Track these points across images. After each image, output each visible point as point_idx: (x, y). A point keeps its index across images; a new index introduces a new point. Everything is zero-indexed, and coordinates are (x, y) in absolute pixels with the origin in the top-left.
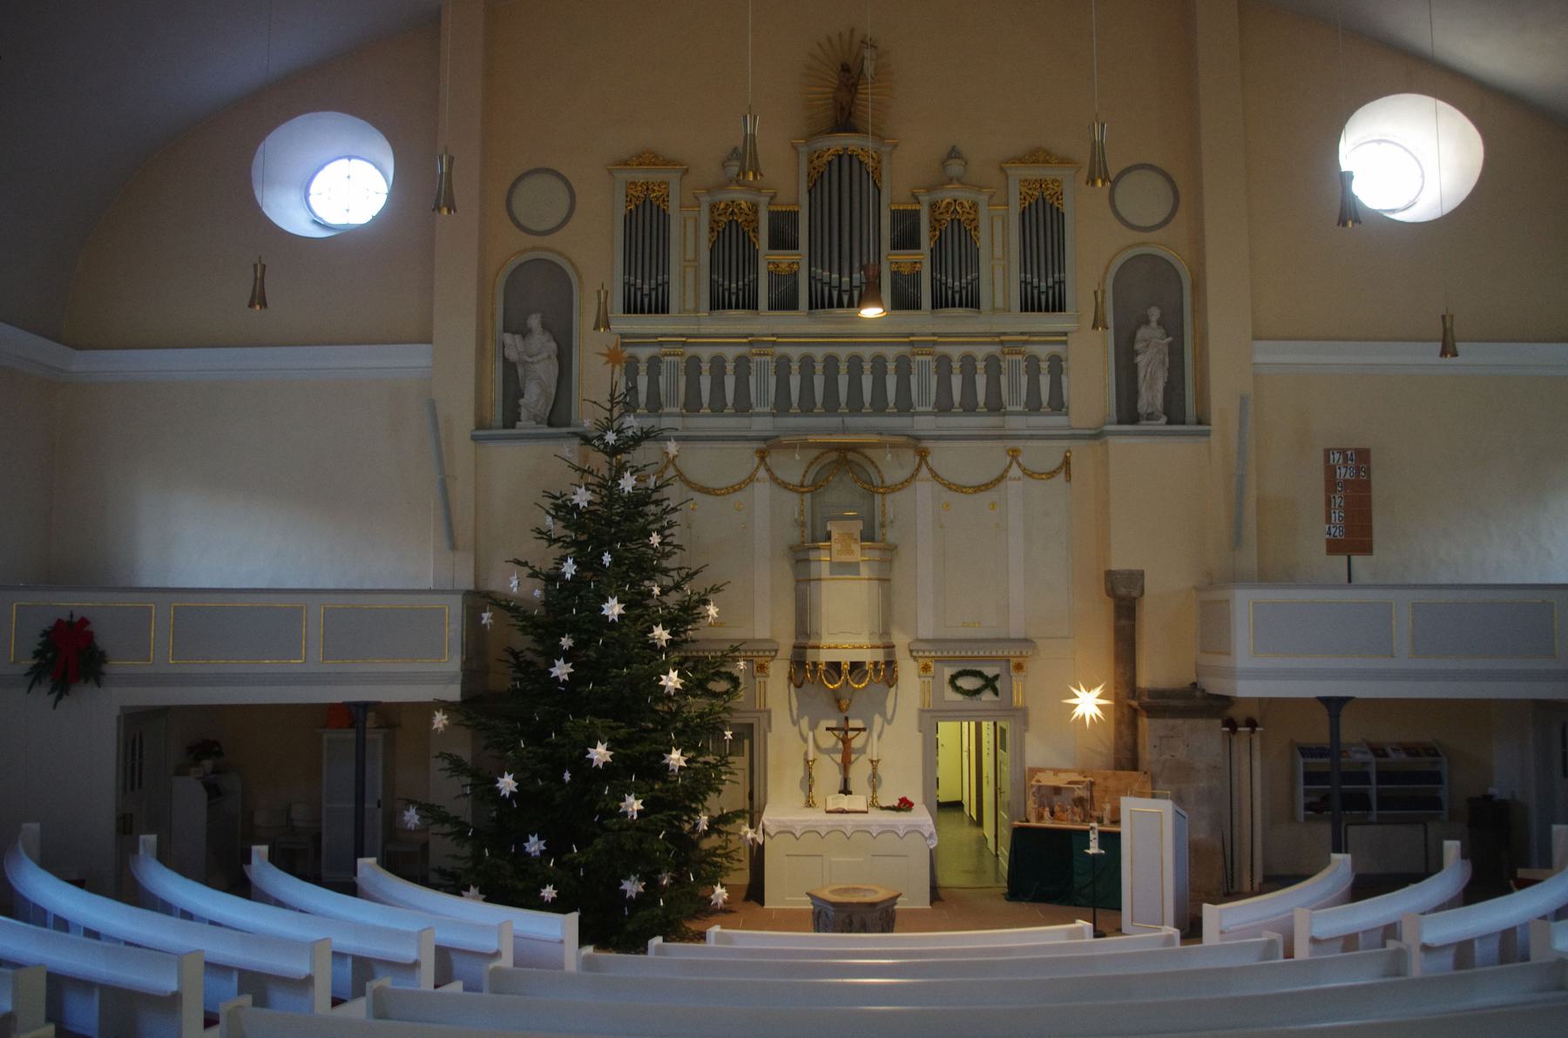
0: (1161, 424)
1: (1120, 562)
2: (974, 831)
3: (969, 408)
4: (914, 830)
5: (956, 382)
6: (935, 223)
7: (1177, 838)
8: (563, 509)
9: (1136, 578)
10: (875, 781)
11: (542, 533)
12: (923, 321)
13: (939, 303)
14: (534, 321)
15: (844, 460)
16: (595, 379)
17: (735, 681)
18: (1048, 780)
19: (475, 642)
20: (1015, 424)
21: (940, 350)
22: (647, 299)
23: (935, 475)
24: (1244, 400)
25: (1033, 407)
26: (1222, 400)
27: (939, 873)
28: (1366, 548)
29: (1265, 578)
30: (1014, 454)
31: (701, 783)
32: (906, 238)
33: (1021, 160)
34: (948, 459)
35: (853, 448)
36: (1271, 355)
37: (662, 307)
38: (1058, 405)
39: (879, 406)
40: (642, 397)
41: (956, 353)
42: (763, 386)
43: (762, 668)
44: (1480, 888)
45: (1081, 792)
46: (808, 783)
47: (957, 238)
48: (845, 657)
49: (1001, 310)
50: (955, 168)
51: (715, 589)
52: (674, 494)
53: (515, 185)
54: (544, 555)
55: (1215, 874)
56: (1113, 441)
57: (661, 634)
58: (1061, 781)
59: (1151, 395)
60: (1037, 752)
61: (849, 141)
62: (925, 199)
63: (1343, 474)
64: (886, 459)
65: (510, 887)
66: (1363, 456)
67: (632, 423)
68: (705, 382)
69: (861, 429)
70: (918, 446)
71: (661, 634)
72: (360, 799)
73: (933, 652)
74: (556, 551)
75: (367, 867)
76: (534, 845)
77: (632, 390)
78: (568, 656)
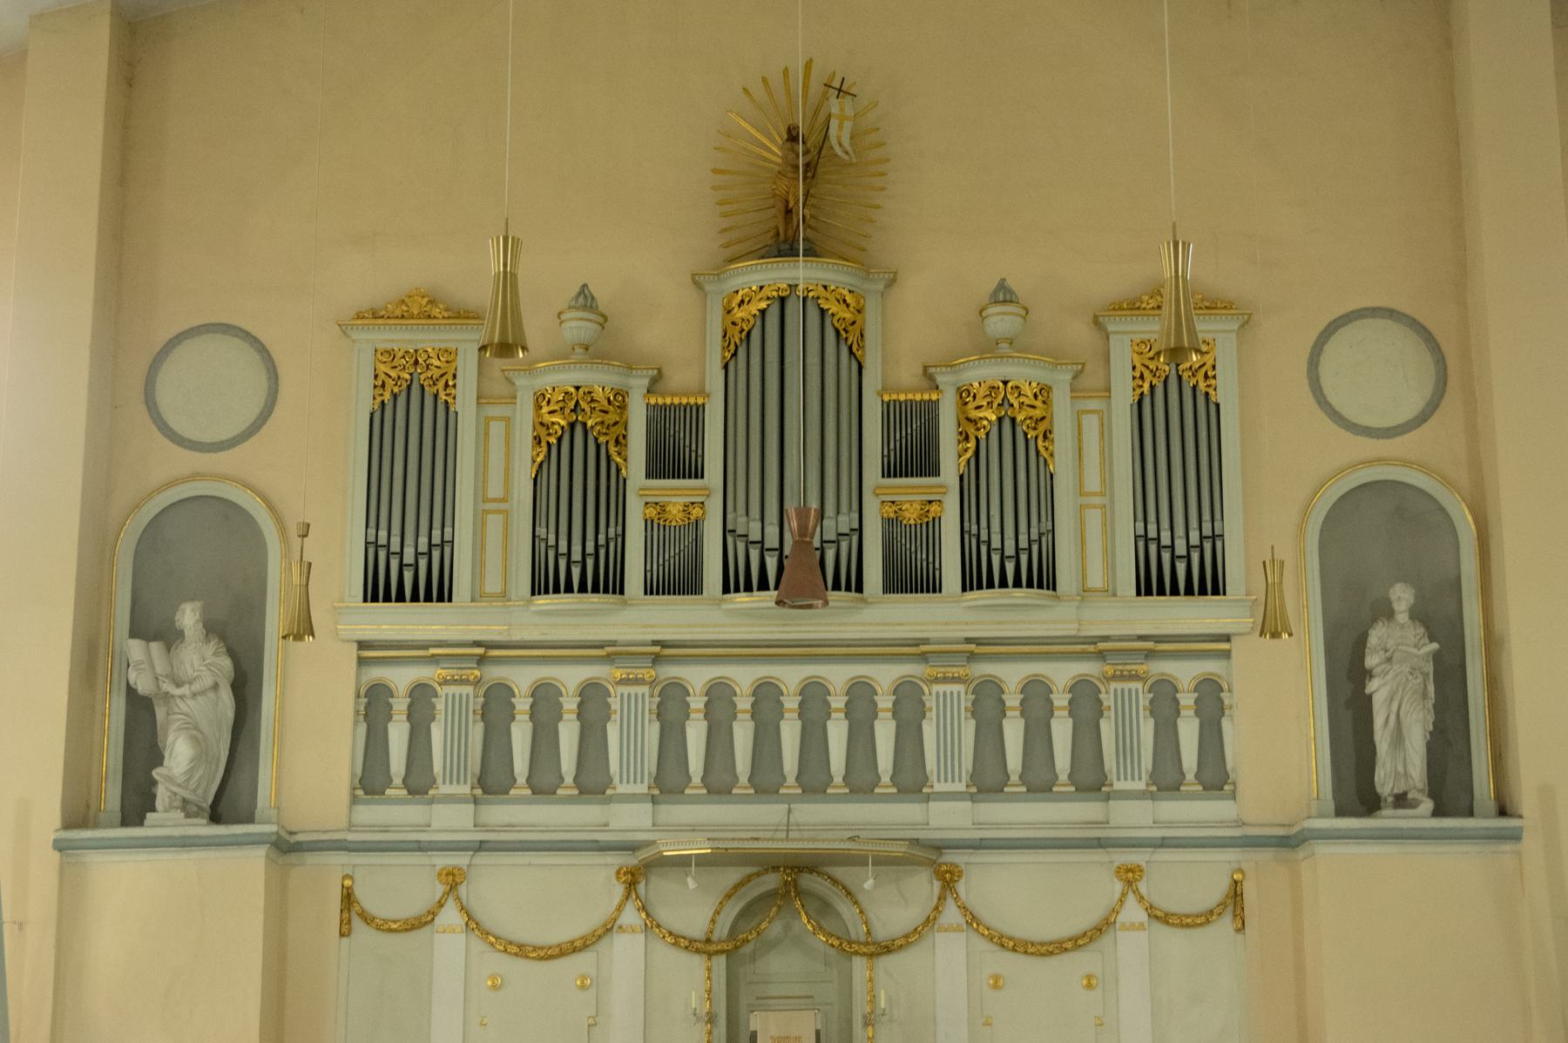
0: (1421, 816)
3: (1039, 786)
6: (967, 423)
13: (971, 581)
14: (189, 617)
20: (451, 818)
21: (495, 673)
23: (473, 923)
25: (1166, 783)
30: (1130, 876)
32: (913, 456)
34: (1011, 892)
37: (437, 590)
38: (1216, 779)
39: (861, 785)
42: (630, 741)
56: (1324, 851)
59: (1402, 759)
61: (801, 273)
70: (937, 859)
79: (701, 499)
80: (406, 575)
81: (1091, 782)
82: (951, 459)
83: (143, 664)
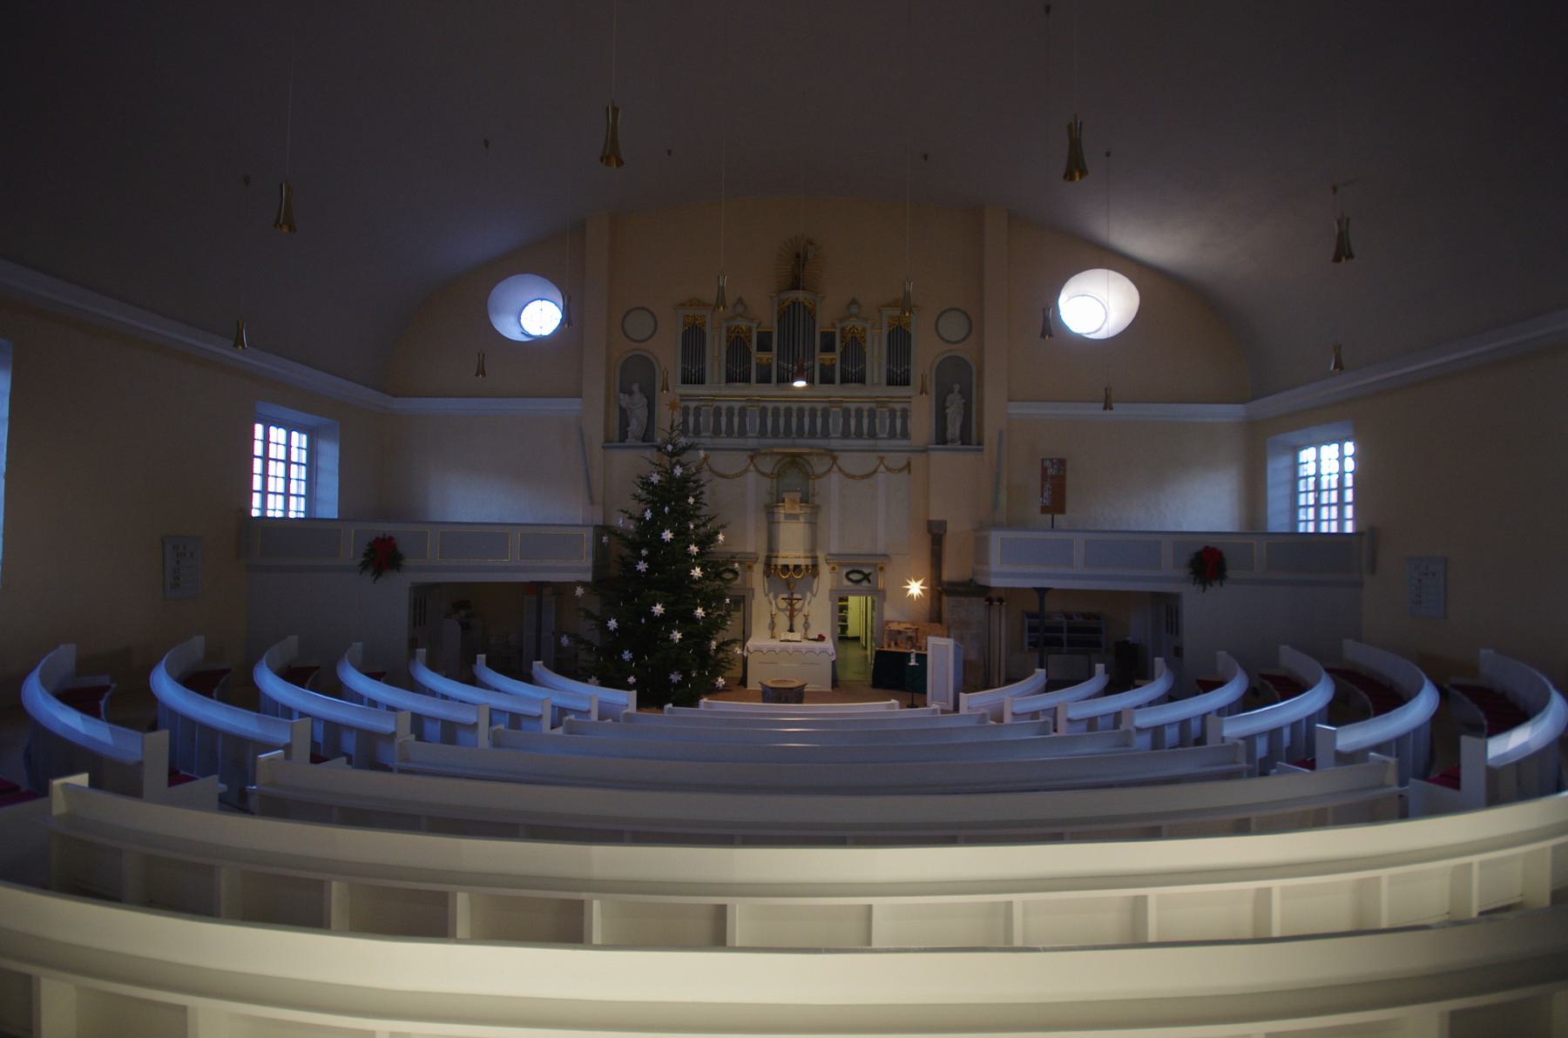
0: (958, 445)
1: (935, 516)
2: (862, 652)
3: (859, 435)
4: (824, 651)
5: (853, 422)
6: (843, 338)
7: (956, 662)
8: (646, 484)
9: (942, 524)
10: (806, 626)
11: (636, 497)
12: (835, 391)
13: (843, 381)
14: (635, 387)
15: (794, 461)
16: (666, 417)
17: (736, 573)
18: (895, 627)
19: (601, 553)
20: (883, 444)
21: (891, 405)
22: (693, 376)
24: (1001, 433)
25: (892, 435)
26: (990, 434)
27: (839, 672)
28: (1062, 511)
29: (1011, 525)
30: (882, 459)
31: (712, 626)
32: (828, 347)
33: (889, 305)
34: (847, 461)
35: (800, 455)
36: (1017, 409)
37: (701, 381)
38: (905, 434)
39: (813, 434)
40: (807, 428)
41: (853, 407)
42: (753, 422)
43: (750, 567)
44: (1111, 689)
45: (910, 633)
46: (772, 626)
47: (854, 348)
48: (791, 562)
49: (876, 386)
50: (854, 310)
51: (723, 526)
52: (705, 476)
53: (628, 313)
54: (635, 507)
55: (976, 676)
56: (932, 453)
57: (694, 549)
58: (901, 627)
59: (954, 430)
60: (889, 613)
61: (800, 295)
62: (838, 326)
63: (1051, 471)
64: (814, 460)
65: (612, 680)
66: (1062, 462)
67: (683, 441)
68: (724, 420)
69: (802, 445)
70: (831, 454)
71: (694, 549)
72: (539, 631)
73: (838, 560)
74: (642, 505)
75: (538, 666)
76: (627, 655)
77: (685, 422)
78: (646, 559)
79: (771, 357)
80: (693, 376)
81: (873, 435)
82: (838, 348)
83: (624, 400)
